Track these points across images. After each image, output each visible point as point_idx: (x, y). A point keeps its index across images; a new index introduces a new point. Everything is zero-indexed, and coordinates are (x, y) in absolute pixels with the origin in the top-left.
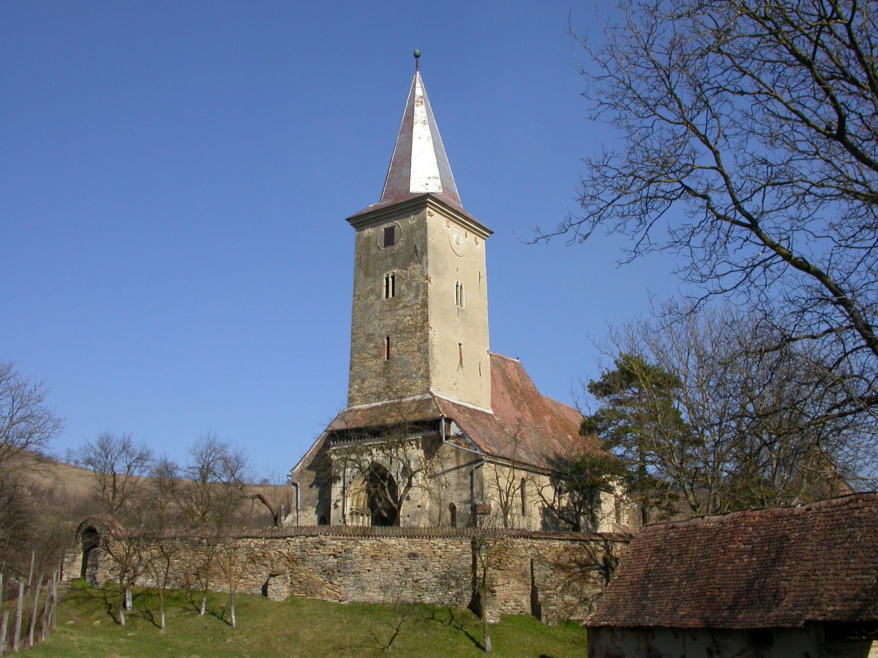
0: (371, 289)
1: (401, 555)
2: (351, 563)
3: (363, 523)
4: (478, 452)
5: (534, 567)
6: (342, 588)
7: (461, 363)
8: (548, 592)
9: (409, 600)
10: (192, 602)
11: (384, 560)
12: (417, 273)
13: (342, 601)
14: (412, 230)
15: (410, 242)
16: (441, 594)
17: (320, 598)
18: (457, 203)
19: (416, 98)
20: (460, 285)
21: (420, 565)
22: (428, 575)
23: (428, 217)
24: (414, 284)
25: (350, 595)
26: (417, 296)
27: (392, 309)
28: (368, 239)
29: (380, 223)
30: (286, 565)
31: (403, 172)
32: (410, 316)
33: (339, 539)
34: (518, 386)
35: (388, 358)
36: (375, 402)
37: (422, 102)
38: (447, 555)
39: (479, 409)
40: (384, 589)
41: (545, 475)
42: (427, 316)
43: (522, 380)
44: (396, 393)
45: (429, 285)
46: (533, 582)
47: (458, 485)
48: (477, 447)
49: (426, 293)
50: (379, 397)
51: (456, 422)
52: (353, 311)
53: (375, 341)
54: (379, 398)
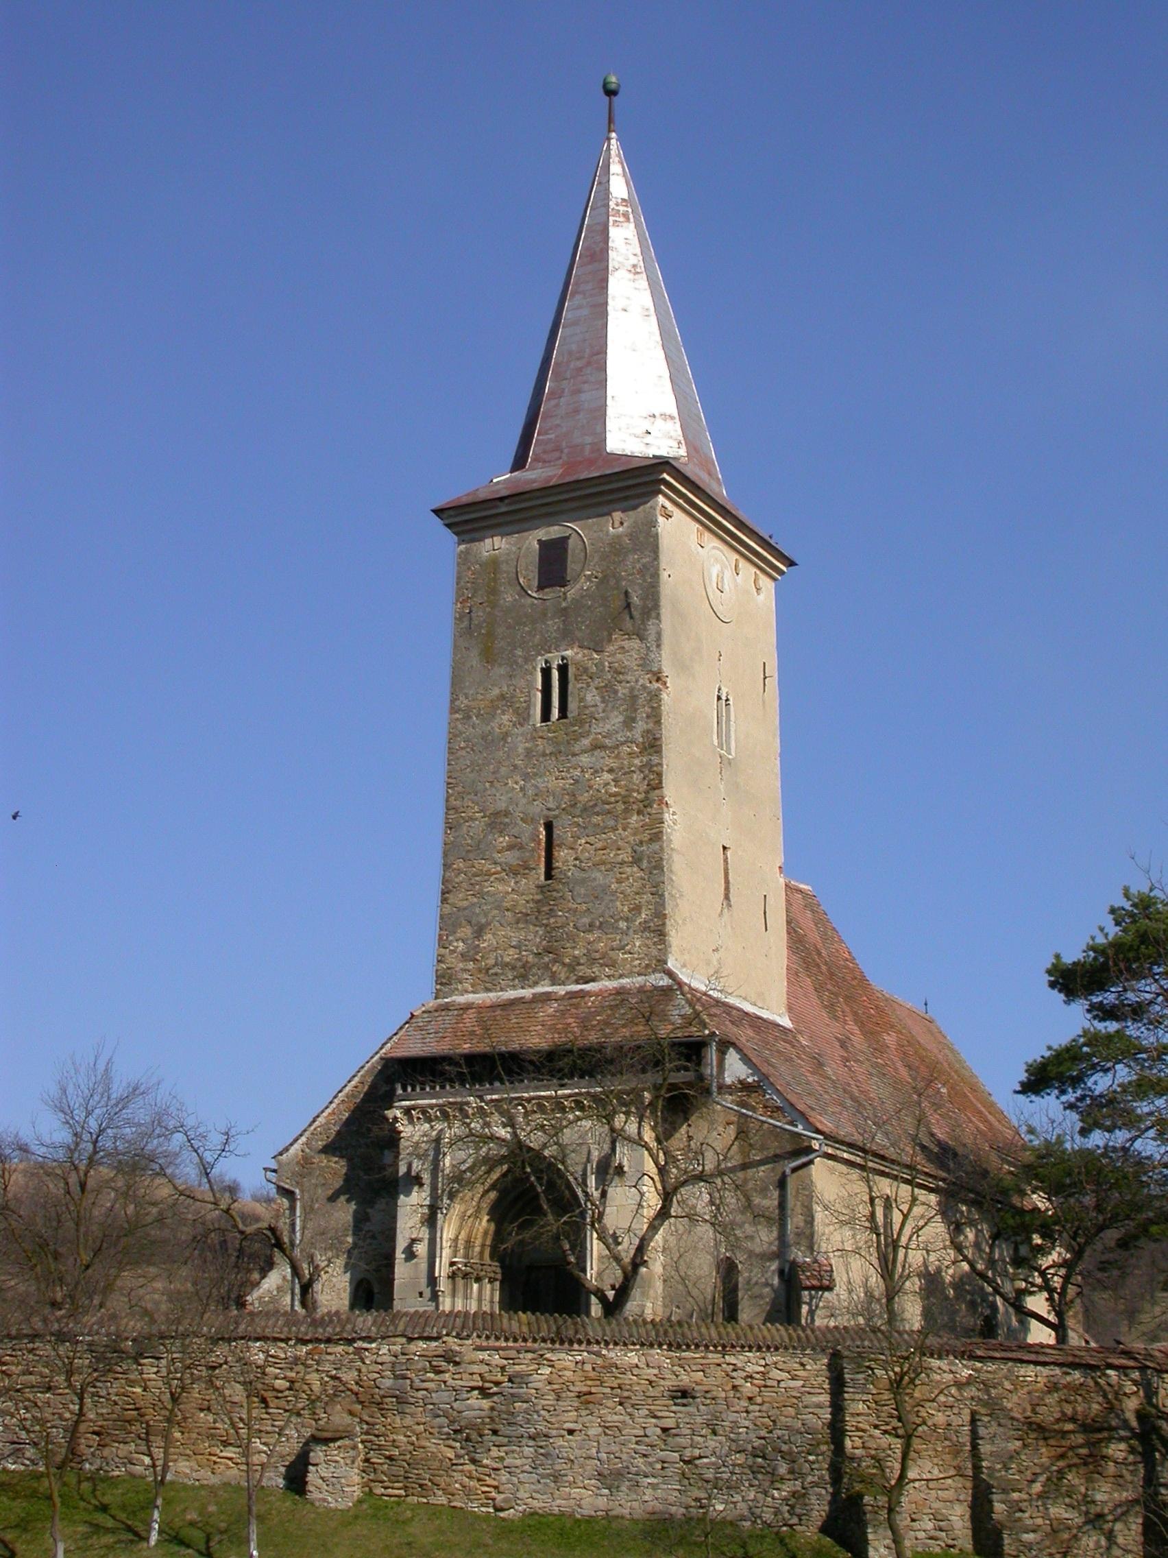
0: (502, 697)
1: (651, 1392)
2: (526, 1412)
3: (480, 1300)
4: (800, 1129)
5: (982, 1431)
6: (504, 1476)
7: (727, 897)
8: (1015, 1495)
9: (673, 1509)
10: (104, 1508)
11: (610, 1403)
12: (631, 661)
13: (502, 1510)
14: (616, 550)
15: (612, 582)
16: (752, 1495)
17: (442, 1500)
18: (714, 485)
19: (612, 204)
20: (724, 698)
21: (699, 1420)
23: (661, 519)
24: (622, 691)
25: (521, 1494)
26: (629, 722)
27: (562, 751)
28: (494, 564)
29: (526, 525)
30: (351, 1413)
31: (583, 397)
32: (611, 771)
33: (497, 1349)
34: (819, 954)
35: (549, 876)
36: (514, 987)
37: (626, 215)
38: (767, 1393)
39: (765, 1014)
40: (610, 1479)
41: (931, 1190)
42: (660, 775)
43: (824, 937)
45: (664, 696)
46: (977, 1468)
48: (795, 1115)
49: (655, 716)
50: (523, 975)
51: (739, 1050)
52: (451, 751)
53: (515, 831)
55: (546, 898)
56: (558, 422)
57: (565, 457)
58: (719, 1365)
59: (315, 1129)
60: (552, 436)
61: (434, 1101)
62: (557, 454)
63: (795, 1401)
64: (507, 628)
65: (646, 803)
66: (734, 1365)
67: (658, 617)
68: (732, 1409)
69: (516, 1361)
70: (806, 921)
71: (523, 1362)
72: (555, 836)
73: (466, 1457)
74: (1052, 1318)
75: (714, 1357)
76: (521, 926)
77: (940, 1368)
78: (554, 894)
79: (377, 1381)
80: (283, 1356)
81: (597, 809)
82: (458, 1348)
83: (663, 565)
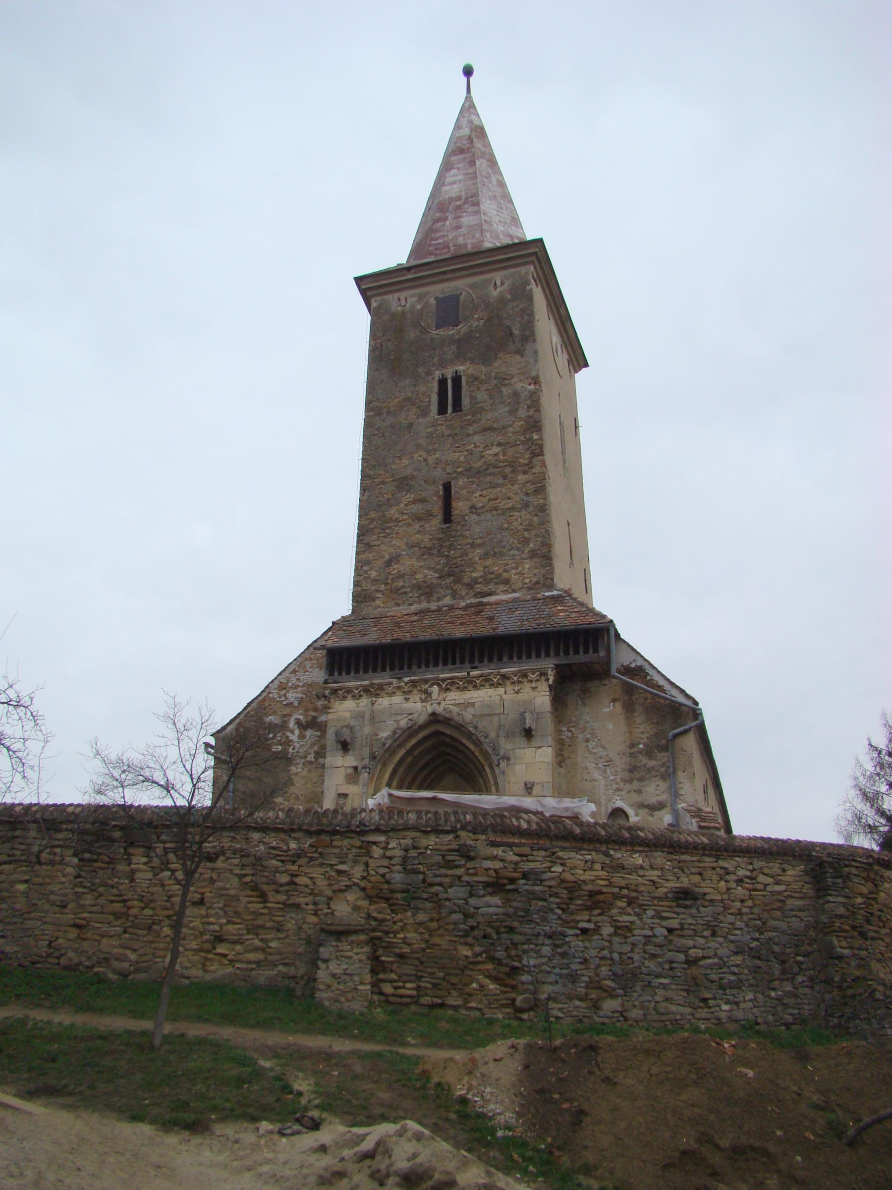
22: (720, 947)
26: (513, 412)
32: (499, 444)
33: (510, 845)
42: (541, 447)
44: (470, 586)
47: (631, 771)
55: (446, 536)
56: (445, 234)
58: (714, 868)
59: (248, 713)
60: (442, 241)
61: (359, 683)
62: (446, 250)
63: (780, 904)
65: (530, 466)
67: (534, 341)
68: (729, 911)
69: (530, 858)
71: (537, 859)
73: (484, 955)
75: (709, 861)
78: (453, 533)
80: (285, 848)
81: (489, 471)
82: (472, 843)
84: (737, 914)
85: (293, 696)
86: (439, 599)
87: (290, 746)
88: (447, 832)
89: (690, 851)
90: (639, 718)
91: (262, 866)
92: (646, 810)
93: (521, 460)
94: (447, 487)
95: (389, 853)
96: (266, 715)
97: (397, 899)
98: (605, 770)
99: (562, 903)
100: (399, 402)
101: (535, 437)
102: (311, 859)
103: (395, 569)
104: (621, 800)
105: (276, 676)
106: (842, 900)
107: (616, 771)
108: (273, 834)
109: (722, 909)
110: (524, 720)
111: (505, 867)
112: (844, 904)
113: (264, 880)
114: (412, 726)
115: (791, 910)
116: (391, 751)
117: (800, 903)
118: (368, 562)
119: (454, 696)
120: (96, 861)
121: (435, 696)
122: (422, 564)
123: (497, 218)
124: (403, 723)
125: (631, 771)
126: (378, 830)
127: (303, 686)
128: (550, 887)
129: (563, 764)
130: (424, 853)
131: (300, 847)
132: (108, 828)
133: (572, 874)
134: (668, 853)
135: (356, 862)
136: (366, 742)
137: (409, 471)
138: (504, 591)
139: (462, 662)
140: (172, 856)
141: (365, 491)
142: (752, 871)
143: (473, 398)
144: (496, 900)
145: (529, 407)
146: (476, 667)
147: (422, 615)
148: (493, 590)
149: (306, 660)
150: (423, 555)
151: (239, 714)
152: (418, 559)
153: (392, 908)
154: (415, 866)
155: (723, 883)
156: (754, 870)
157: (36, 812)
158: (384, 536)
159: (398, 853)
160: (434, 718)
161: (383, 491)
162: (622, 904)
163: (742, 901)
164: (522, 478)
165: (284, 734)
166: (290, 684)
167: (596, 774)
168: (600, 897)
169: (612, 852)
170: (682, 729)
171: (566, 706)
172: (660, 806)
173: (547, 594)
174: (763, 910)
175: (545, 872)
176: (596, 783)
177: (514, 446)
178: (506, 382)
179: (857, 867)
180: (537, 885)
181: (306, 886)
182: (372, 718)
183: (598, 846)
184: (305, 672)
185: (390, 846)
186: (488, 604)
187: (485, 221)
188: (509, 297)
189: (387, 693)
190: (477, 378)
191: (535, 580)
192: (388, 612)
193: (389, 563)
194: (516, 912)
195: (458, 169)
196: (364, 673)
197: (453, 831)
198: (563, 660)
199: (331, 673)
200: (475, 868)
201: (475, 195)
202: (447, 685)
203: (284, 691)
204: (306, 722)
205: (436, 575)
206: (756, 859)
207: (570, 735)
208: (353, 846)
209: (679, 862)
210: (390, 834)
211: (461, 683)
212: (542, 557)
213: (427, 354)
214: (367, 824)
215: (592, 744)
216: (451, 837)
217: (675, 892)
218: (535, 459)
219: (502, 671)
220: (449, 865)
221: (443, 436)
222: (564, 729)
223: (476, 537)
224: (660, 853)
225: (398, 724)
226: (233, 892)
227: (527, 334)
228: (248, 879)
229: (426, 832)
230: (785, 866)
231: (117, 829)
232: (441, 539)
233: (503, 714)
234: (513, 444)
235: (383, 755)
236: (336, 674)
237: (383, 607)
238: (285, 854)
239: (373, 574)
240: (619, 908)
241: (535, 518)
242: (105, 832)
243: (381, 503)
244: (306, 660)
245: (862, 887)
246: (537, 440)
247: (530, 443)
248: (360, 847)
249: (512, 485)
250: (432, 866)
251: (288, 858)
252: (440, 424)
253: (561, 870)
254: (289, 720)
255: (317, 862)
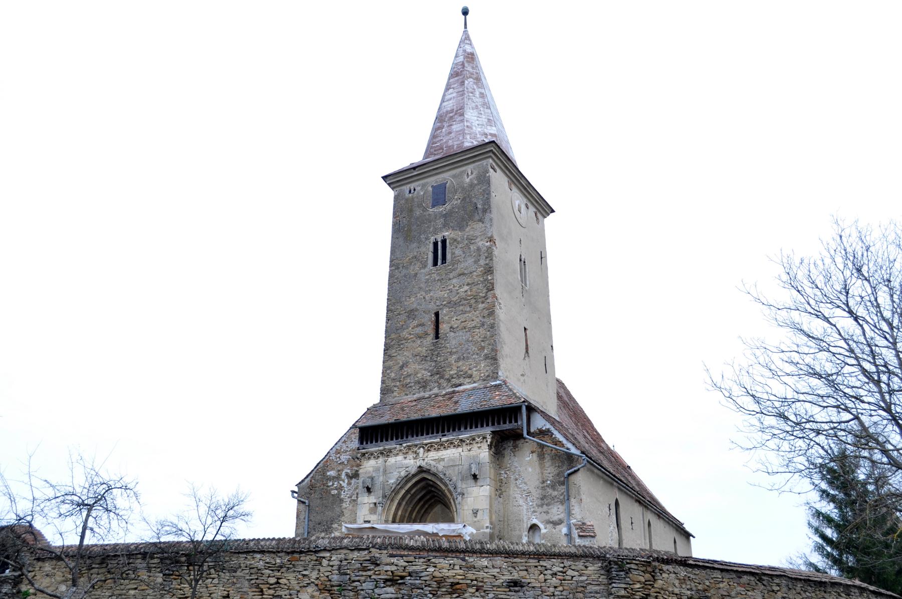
11: (470, 590)
31: (453, 127)
32: (468, 284)
33: (402, 556)
42: (493, 284)
44: (449, 380)
47: (542, 499)
54: (424, 387)
56: (442, 138)
57: (445, 151)
58: (536, 567)
60: (439, 144)
61: (377, 449)
62: (441, 151)
63: (583, 589)
64: (417, 226)
66: (545, 566)
68: (545, 594)
69: (414, 563)
70: (562, 392)
71: (418, 564)
72: (440, 318)
74: (872, 361)
75: (533, 562)
76: (423, 362)
77: (668, 570)
79: (329, 577)
81: (461, 303)
83: (492, 190)
84: (551, 596)
85: (344, 458)
86: (431, 390)
87: (342, 490)
88: (364, 550)
89: (520, 556)
90: (548, 463)
91: (262, 574)
92: (552, 525)
93: (481, 294)
94: (437, 315)
95: (331, 563)
96: (328, 471)
97: (334, 590)
98: (527, 499)
99: (433, 591)
100: (409, 259)
101: (490, 278)
102: (288, 568)
103: (405, 371)
104: (536, 518)
105: (333, 445)
106: (624, 586)
107: (533, 499)
108: (267, 555)
109: (541, 592)
110: (470, 468)
111: (398, 569)
112: (625, 589)
113: (262, 582)
114: (407, 475)
115: (590, 593)
116: (396, 492)
117: (597, 588)
118: (390, 368)
119: (433, 455)
120: (172, 575)
121: (421, 455)
122: (420, 367)
123: (477, 122)
124: (403, 474)
125: (542, 499)
126: (325, 550)
127: (350, 451)
128: (426, 581)
129: (502, 496)
130: (351, 562)
131: (282, 562)
132: (179, 555)
133: (440, 572)
134: (505, 557)
135: (313, 569)
136: (380, 487)
137: (415, 306)
138: (469, 383)
139: (438, 432)
140: (212, 571)
141: (389, 320)
142: (563, 568)
143: (453, 254)
144: (391, 590)
145: (486, 258)
146: (445, 435)
147: (418, 401)
148: (462, 382)
149: (352, 434)
150: (422, 361)
151: (313, 471)
152: (419, 364)
153: (332, 596)
154: (345, 571)
155: (542, 575)
156: (565, 567)
157: (141, 548)
158: (399, 350)
159: (337, 563)
160: (421, 470)
161: (399, 320)
162: (472, 590)
163: (555, 587)
164: (481, 306)
165: (338, 482)
166: (342, 450)
167: (521, 502)
168: (458, 586)
169: (467, 558)
170: (572, 470)
171: (504, 457)
172: (560, 522)
173: (493, 384)
174: (570, 593)
175: (422, 572)
176: (521, 508)
177: (477, 285)
178: (473, 241)
179: (637, 564)
180: (417, 580)
181: (285, 584)
182: (385, 471)
183: (458, 554)
184: (351, 442)
185: (332, 559)
186: (458, 392)
187: (467, 126)
188: (476, 182)
189: (394, 454)
190: (455, 240)
191: (487, 374)
192: (401, 400)
193: (402, 367)
194: (403, 597)
195: (453, 88)
196: (381, 442)
197: (367, 549)
198: (497, 428)
199: (362, 443)
200: (380, 571)
201: (462, 108)
202: (428, 448)
203: (339, 455)
204: (352, 474)
205: (429, 374)
206: (566, 560)
207: (506, 476)
208: (312, 560)
209: (512, 563)
210: (332, 552)
211: (436, 446)
212: (492, 358)
213: (426, 225)
214: (319, 546)
215: (519, 482)
216: (366, 552)
217: (508, 582)
218: (489, 293)
219: (460, 437)
220: (365, 569)
221: (435, 280)
222: (503, 472)
223: (453, 347)
224: (499, 558)
225: (400, 474)
226: (244, 590)
227: (486, 208)
228: (253, 582)
229: (352, 550)
230: (587, 564)
231: (184, 556)
232: (432, 350)
233: (461, 465)
234: (476, 283)
235: (391, 494)
236: (365, 443)
237: (398, 397)
238: (274, 566)
239: (393, 375)
240: (470, 593)
241: (488, 333)
242: (177, 558)
243: (398, 328)
244: (352, 434)
245: (641, 577)
246: (490, 280)
247: (486, 282)
248: (316, 560)
249: (475, 311)
250: (355, 570)
251: (275, 568)
252: (433, 273)
253: (433, 570)
254: (342, 474)
255: (291, 570)
